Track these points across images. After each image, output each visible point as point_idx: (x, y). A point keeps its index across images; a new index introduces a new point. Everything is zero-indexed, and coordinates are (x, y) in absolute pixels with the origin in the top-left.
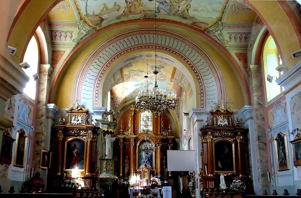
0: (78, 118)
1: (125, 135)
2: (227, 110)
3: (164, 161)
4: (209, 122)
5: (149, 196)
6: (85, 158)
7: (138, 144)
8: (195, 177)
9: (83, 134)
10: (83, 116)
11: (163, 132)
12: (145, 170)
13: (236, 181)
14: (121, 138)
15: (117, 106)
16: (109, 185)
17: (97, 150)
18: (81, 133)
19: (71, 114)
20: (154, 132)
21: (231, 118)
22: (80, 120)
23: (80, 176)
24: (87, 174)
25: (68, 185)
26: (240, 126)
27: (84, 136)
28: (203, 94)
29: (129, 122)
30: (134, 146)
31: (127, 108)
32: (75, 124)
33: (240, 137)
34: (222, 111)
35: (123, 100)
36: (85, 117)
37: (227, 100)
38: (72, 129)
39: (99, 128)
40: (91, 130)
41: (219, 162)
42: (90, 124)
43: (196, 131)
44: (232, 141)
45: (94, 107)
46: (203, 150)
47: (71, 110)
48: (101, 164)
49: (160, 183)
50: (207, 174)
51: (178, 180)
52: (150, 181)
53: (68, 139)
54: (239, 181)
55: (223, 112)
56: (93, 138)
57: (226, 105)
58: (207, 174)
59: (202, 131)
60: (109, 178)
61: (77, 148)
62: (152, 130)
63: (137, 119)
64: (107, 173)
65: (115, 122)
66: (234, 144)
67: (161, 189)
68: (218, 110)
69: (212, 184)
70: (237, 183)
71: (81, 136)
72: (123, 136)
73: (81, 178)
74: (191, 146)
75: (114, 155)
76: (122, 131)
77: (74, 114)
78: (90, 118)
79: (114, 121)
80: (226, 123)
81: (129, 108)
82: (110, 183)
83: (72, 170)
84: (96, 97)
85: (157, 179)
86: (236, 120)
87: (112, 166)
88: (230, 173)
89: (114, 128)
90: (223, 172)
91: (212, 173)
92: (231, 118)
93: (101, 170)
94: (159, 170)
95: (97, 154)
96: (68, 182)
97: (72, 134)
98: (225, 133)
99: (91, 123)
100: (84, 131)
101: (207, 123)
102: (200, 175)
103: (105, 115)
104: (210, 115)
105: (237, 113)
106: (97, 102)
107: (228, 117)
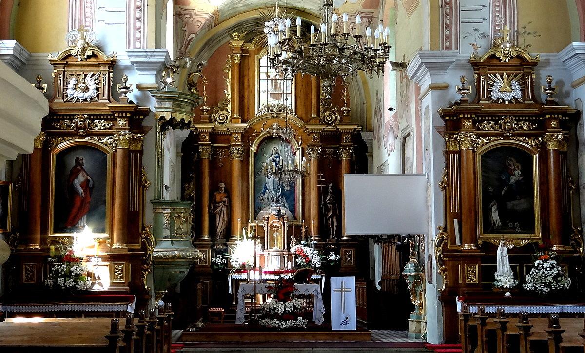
0: (84, 83)
1: (216, 121)
2: (519, 57)
3: (328, 198)
4: (466, 91)
5: (291, 305)
6: (108, 198)
7: (253, 148)
8: (424, 250)
9: (101, 129)
10: (101, 75)
11: (324, 111)
12: (276, 222)
13: (543, 264)
14: (203, 132)
15: (193, 35)
16: (180, 276)
17: (144, 175)
18: (96, 126)
19: (64, 71)
20: (298, 113)
21: (532, 79)
22: (92, 87)
23: (99, 251)
24: (116, 245)
25: (63, 279)
26: (557, 104)
27: (105, 135)
28: (451, 9)
29: (228, 84)
30: (241, 154)
31: (219, 41)
32: (79, 99)
33: (557, 137)
34: (506, 57)
35: (208, 20)
36: (107, 79)
37: (522, 24)
38: (70, 115)
39: (147, 112)
40: (126, 117)
41: (493, 209)
42: (122, 99)
43: (427, 118)
44: (532, 146)
45: (132, 49)
46: (447, 175)
47: (64, 59)
48: (156, 214)
49: (316, 261)
50: (458, 243)
51: (369, 251)
52: (289, 254)
53: (57, 145)
54: (551, 264)
55: (507, 61)
56: (131, 141)
57: (516, 40)
58: (458, 243)
59: (447, 118)
60: (179, 258)
61: (85, 171)
62: (293, 106)
63: (251, 74)
64: (172, 244)
65: (193, 93)
66: (537, 155)
67: (319, 277)
68: (493, 57)
69: (473, 272)
70: (546, 270)
71: (96, 135)
72: (209, 126)
73: (100, 259)
74: (410, 156)
75: (185, 179)
76: (208, 110)
77: (73, 69)
78: (120, 82)
79: (190, 90)
80: (518, 93)
81: (225, 41)
82: (183, 272)
83: (73, 235)
84: (138, 19)
85: (308, 248)
86: (544, 83)
87: (186, 221)
88: (525, 239)
89: (192, 109)
90: (506, 236)
91: (474, 241)
92: (532, 79)
93: (156, 234)
94: (314, 224)
95: (145, 186)
96: (63, 270)
97: (69, 130)
98: (511, 123)
99: (123, 95)
100: (105, 120)
101: (461, 94)
102: (438, 245)
103: (164, 72)
104: (471, 69)
105: (549, 63)
106: (140, 32)
107: (523, 75)
